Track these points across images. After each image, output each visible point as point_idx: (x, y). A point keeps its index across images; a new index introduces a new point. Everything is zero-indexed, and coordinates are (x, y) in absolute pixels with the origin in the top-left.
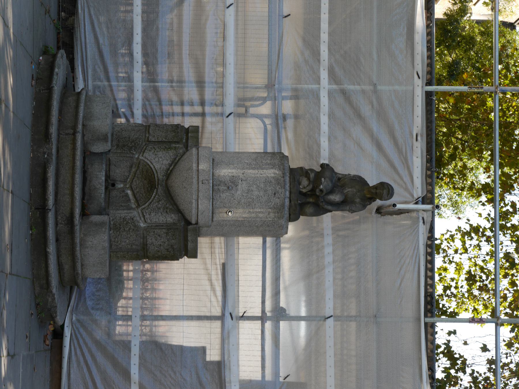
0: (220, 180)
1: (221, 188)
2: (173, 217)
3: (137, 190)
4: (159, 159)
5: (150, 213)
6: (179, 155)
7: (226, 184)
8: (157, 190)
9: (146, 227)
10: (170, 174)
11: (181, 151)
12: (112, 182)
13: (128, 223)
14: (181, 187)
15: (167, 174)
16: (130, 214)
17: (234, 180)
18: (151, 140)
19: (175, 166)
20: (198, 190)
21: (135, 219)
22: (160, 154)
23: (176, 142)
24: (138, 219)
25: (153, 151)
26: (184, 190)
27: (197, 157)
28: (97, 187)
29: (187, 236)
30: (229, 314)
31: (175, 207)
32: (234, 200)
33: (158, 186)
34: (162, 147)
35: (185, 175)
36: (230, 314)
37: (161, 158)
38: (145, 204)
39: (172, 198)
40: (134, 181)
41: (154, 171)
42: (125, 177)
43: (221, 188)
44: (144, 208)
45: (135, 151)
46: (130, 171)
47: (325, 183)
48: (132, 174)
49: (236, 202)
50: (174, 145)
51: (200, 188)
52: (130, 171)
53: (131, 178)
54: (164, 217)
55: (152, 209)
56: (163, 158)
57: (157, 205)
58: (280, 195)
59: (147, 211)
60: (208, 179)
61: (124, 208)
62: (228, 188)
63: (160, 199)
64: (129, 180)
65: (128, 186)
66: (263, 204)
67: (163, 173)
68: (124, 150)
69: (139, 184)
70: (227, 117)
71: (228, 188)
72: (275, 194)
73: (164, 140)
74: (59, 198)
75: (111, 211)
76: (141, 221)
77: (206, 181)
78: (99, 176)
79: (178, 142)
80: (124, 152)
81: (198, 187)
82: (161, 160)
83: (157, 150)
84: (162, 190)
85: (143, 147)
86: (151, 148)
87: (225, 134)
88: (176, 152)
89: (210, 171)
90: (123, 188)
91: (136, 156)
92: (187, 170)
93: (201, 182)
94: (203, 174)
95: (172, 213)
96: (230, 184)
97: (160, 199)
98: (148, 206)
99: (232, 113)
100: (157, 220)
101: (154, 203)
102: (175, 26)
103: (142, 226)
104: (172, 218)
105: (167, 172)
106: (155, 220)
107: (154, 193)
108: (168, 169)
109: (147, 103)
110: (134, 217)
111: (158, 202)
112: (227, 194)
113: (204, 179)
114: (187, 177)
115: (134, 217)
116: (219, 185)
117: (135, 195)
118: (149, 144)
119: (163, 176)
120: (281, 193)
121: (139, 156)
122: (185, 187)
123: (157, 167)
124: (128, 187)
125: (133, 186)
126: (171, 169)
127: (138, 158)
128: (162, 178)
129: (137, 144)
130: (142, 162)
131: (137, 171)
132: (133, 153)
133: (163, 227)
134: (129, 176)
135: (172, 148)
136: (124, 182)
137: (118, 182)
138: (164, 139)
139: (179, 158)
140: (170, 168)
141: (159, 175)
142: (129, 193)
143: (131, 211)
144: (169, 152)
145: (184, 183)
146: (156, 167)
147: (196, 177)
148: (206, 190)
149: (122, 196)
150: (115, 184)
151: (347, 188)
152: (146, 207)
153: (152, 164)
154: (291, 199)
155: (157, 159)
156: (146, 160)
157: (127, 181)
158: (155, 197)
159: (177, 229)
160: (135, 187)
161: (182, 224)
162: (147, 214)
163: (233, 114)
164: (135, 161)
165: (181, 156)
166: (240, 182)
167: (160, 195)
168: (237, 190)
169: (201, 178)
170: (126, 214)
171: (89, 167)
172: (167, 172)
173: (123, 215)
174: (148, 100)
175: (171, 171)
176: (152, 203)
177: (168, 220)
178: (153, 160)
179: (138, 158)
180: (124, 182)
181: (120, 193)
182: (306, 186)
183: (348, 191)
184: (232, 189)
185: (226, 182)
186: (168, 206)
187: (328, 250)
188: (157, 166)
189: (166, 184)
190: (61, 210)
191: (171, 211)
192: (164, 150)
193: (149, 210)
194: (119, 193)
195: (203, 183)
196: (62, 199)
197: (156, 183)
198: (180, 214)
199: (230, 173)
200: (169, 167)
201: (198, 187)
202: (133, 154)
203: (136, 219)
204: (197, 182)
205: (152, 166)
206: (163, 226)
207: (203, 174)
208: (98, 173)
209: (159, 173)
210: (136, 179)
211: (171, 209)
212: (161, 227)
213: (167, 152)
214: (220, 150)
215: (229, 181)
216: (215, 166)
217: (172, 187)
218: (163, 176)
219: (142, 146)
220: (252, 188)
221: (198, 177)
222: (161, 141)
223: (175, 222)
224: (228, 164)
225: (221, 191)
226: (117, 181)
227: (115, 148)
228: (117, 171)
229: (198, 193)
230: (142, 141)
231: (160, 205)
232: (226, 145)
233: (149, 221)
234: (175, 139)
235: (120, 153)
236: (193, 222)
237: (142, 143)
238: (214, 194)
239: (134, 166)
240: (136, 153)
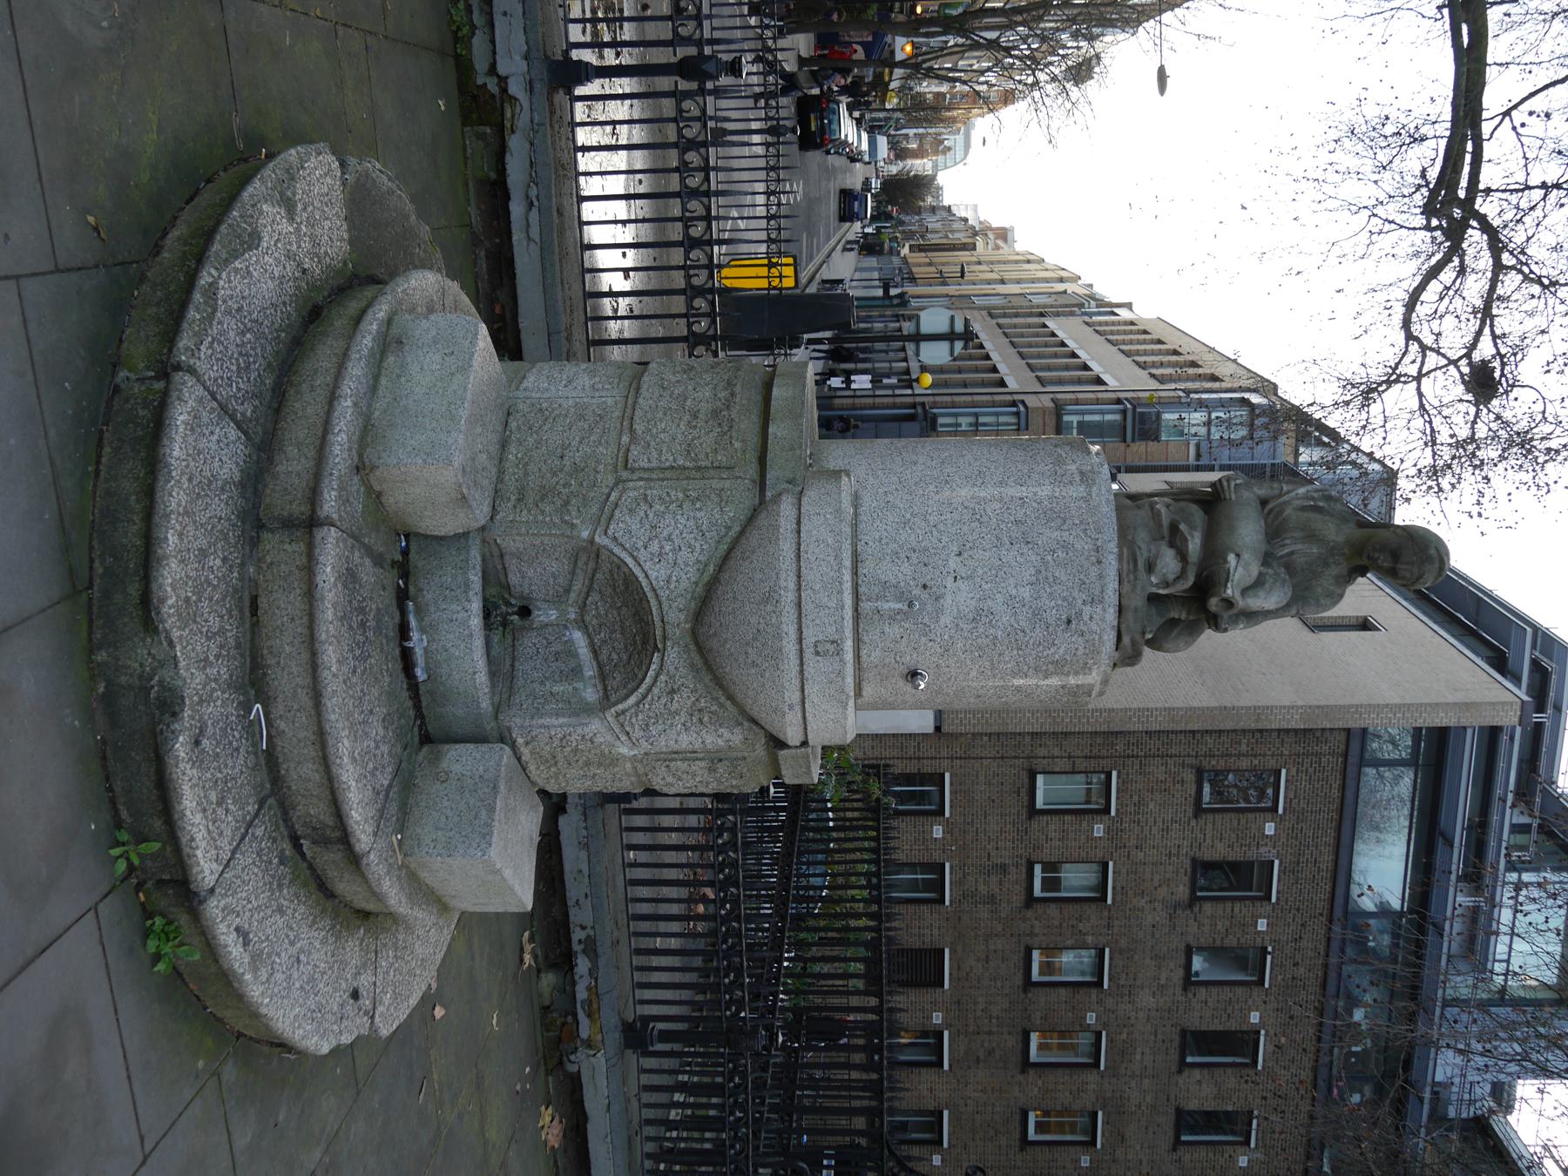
4: (662, 547)
24: (609, 738)
37: (669, 538)
38: (627, 697)
43: (886, 606)
44: (623, 712)
47: (1240, 569)
49: (939, 650)
51: (809, 670)
58: (1085, 624)
63: (676, 687)
66: (1027, 651)
68: (543, 512)
71: (911, 605)
72: (1069, 622)
76: (618, 743)
77: (828, 646)
80: (540, 518)
82: (667, 548)
89: (843, 607)
91: (585, 534)
93: (812, 650)
94: (818, 622)
98: (637, 704)
102: (508, 315)
107: (653, 667)
111: (668, 693)
112: (907, 626)
113: (821, 637)
114: (761, 627)
120: (1091, 618)
122: (754, 664)
123: (657, 578)
125: (587, 618)
130: (604, 552)
146: (652, 574)
151: (1288, 541)
152: (630, 708)
154: (1123, 627)
156: (617, 550)
159: (745, 758)
160: (595, 622)
166: (949, 582)
168: (939, 612)
169: (810, 636)
182: (1171, 577)
183: (1292, 553)
185: (902, 584)
188: (658, 573)
195: (817, 653)
197: (658, 633)
210: (594, 597)
220: (989, 602)
231: (675, 706)
236: (793, 735)
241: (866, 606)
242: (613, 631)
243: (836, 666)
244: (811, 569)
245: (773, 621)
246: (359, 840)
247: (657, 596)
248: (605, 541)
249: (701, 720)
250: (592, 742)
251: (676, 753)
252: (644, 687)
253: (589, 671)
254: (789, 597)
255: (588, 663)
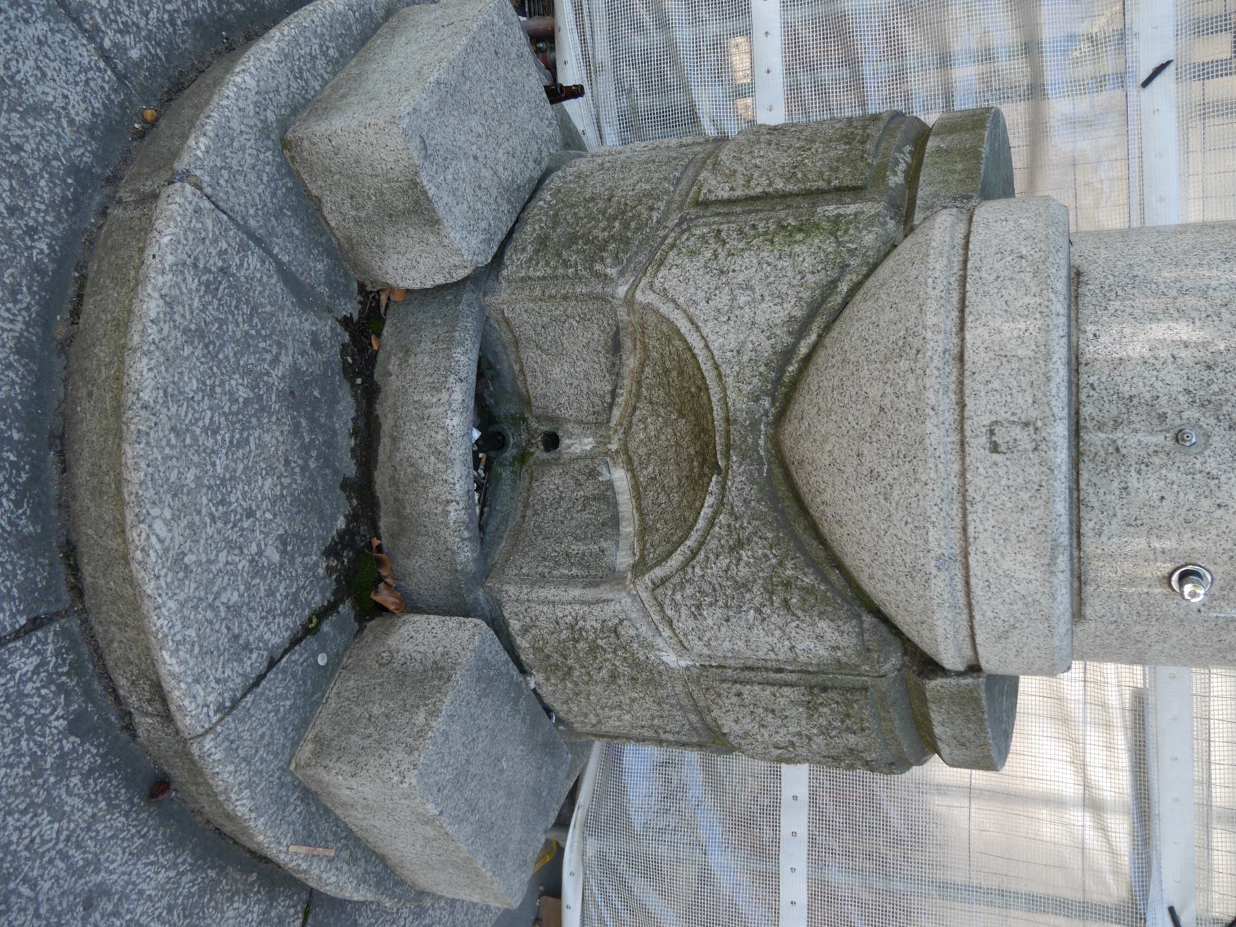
0: (1126, 390)
1: (1132, 440)
2: (828, 635)
3: (650, 469)
4: (733, 299)
5: (699, 607)
6: (853, 262)
7: (1163, 417)
8: (725, 479)
9: (695, 671)
10: (795, 384)
11: (869, 239)
12: (545, 428)
13: (594, 649)
14: (849, 470)
15: (777, 381)
16: (596, 610)
17: (1215, 387)
18: (712, 197)
19: (827, 328)
20: (963, 492)
21: (627, 631)
22: (746, 266)
23: (842, 192)
24: (644, 630)
25: (708, 254)
26: (871, 489)
27: (957, 267)
28: (425, 469)
29: (927, 718)
30: (1166, 913)
31: (834, 576)
32: (1220, 512)
33: (727, 457)
34: (761, 227)
35: (874, 392)
36: (1171, 910)
37: (748, 287)
38: (670, 554)
39: (814, 528)
40: (635, 420)
41: (706, 367)
42: (596, 400)
43: (1132, 440)
44: (664, 581)
45: (617, 260)
46: (615, 371)
48: (626, 382)
50: (832, 210)
51: (978, 483)
52: (615, 371)
53: (627, 405)
54: (778, 633)
55: (706, 588)
56: (759, 289)
57: (728, 567)
59: (678, 597)
60: (1033, 413)
61: (574, 571)
62: (1179, 438)
64: (616, 412)
65: (614, 447)
67: (755, 380)
69: (657, 438)
70: (1145, 84)
71: (1179, 438)
73: (780, 184)
74: (89, 580)
75: (511, 590)
77: (1017, 432)
78: (433, 411)
79: (855, 191)
80: (561, 271)
81: (963, 474)
82: (742, 300)
83: (734, 243)
84: (751, 480)
85: (665, 237)
86: (703, 236)
87: (1135, 163)
88: (839, 243)
89: (1048, 358)
90: (591, 456)
91: (622, 291)
92: (887, 359)
93: (983, 440)
94: (996, 384)
95: (821, 615)
96: (1193, 413)
97: (744, 535)
98: (683, 568)
99: (1168, 63)
100: (741, 644)
101: (712, 557)
103: (673, 665)
104: (820, 637)
105: (781, 370)
106: (727, 645)
107: (710, 500)
108: (788, 353)
109: (804, 78)
110: (621, 621)
111: (731, 549)
112: (1172, 476)
113: (1003, 415)
114: (887, 401)
115: (621, 621)
116: (1117, 424)
117: (639, 493)
118: (698, 217)
119: (757, 399)
121: (634, 287)
122: (873, 475)
123: (722, 346)
124: (617, 452)
125: (632, 445)
126: (803, 350)
127: (629, 301)
128: (750, 412)
129: (633, 225)
131: (643, 365)
132: (606, 276)
133: (779, 676)
134: (613, 394)
135: (817, 226)
136: (598, 424)
137: (569, 426)
138: (778, 180)
139: (854, 278)
140: (795, 345)
141: (732, 395)
142: (617, 484)
143: (603, 592)
144: (797, 249)
145: (866, 448)
147: (946, 403)
148: (1025, 495)
149: (586, 498)
150: (560, 434)
153: (698, 329)
155: (722, 299)
156: (666, 309)
157: (608, 421)
158: (711, 523)
159: (865, 689)
160: (642, 451)
161: (888, 666)
162: (683, 610)
163: (1170, 70)
164: (622, 314)
165: (865, 270)
167: (740, 508)
169: (980, 413)
170: (577, 607)
171: (393, 366)
172: (781, 370)
173: (566, 613)
174: (811, 68)
175: (808, 359)
176: (702, 553)
177: (799, 646)
178: (703, 303)
179: (629, 301)
180: (598, 422)
181: (579, 484)
184: (1207, 445)
185: (1163, 400)
186: (789, 573)
187: (1184, 331)
189: (776, 443)
190: (116, 645)
191: (812, 600)
192: (772, 242)
193: (689, 591)
194: (572, 482)
195: (995, 448)
196: (102, 582)
197: (719, 440)
198: (868, 620)
199: (1186, 345)
200: (790, 340)
201: (963, 474)
202: (606, 278)
203: (632, 632)
204: (955, 437)
205: (697, 345)
206: (780, 670)
207: (996, 384)
208: (426, 398)
209: (730, 381)
211: (809, 590)
212: (772, 675)
213: (787, 249)
214: (1113, 220)
215: (1181, 398)
216: (1087, 311)
217: (801, 463)
218: (757, 399)
219: (662, 233)
221: (962, 405)
222: (765, 196)
223: (845, 660)
224: (1174, 293)
225: (1132, 460)
226: (567, 421)
227: (524, 257)
228: (556, 373)
229: (965, 516)
230: (669, 203)
231: (744, 571)
232: (1142, 208)
233: (699, 647)
234: (845, 177)
235: (544, 278)
236: (951, 658)
237: (666, 214)
238: (1085, 476)
239: (628, 344)
240: (622, 273)
241: (1094, 439)
242: (665, 461)
243: (1033, 473)
244: (986, 294)
245: (910, 388)
246: (180, 708)
247: (720, 375)
248: (651, 298)
249: (786, 604)
250: (618, 636)
251: (751, 669)
252: (695, 536)
253: (628, 528)
254: (938, 342)
255: (628, 515)
